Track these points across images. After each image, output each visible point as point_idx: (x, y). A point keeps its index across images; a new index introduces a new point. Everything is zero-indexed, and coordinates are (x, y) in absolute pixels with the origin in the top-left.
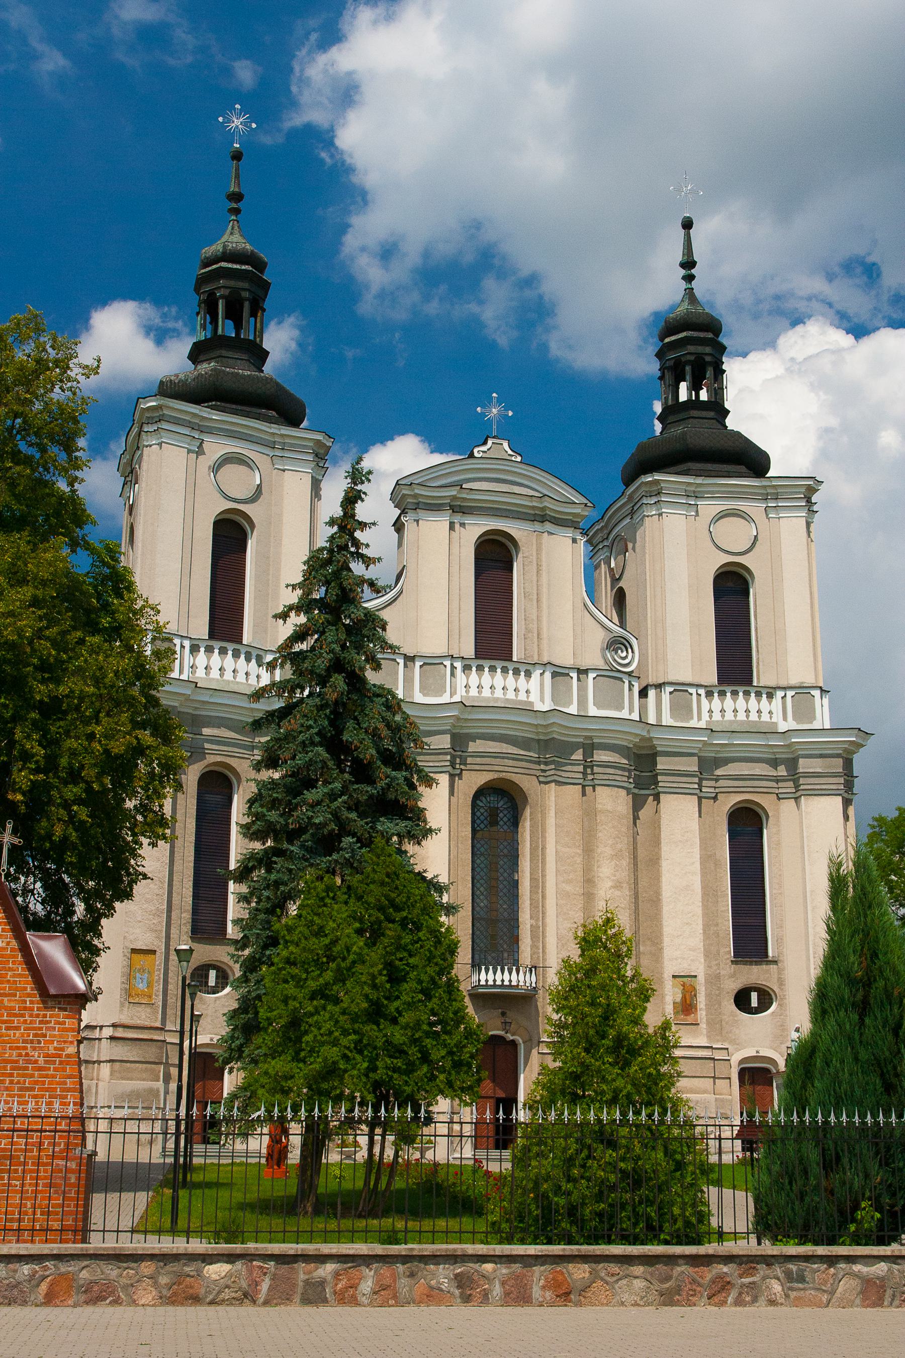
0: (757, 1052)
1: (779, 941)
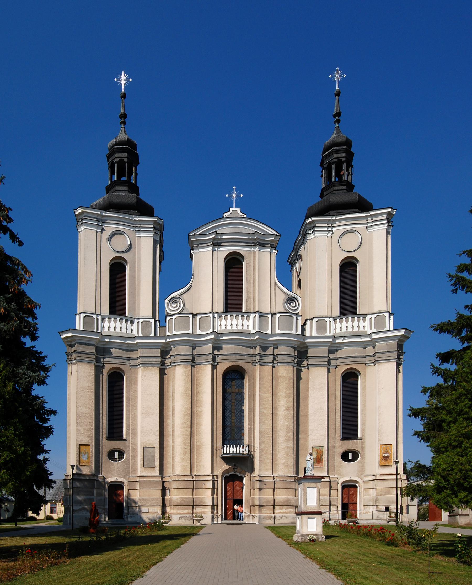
0: (117, 479)
1: (363, 430)
